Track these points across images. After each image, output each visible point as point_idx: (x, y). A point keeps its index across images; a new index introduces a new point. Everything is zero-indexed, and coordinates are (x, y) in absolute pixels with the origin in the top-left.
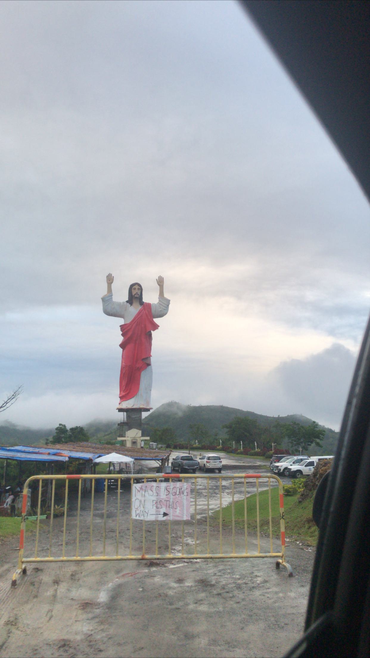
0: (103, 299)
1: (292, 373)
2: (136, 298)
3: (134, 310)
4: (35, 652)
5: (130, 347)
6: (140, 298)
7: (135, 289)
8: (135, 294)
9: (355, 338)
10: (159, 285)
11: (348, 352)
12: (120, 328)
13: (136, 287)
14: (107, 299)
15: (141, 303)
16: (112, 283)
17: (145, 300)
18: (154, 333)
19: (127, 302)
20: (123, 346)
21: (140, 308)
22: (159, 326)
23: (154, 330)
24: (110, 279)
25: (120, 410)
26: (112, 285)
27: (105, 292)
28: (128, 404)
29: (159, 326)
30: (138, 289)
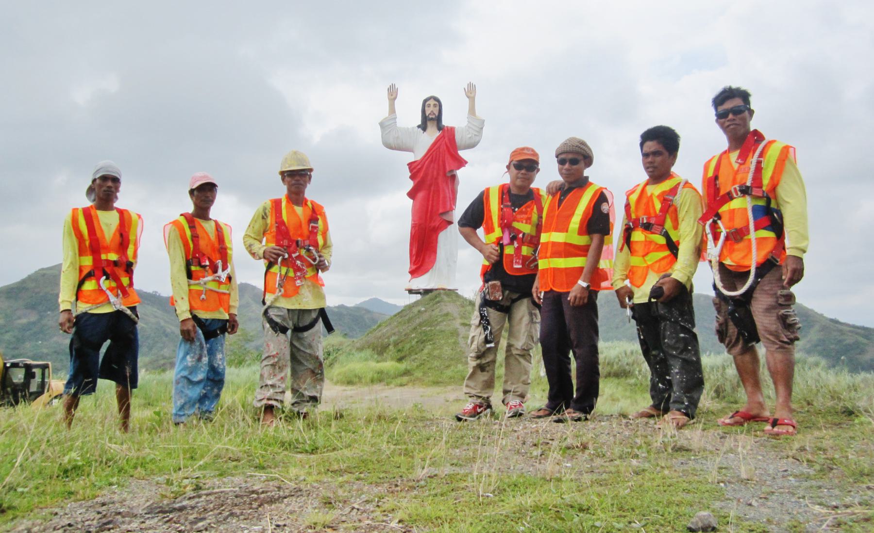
0: (382, 125)
1: (85, 399)
2: (432, 119)
3: (431, 136)
4: (618, 344)
5: (421, 195)
6: (438, 119)
7: (429, 106)
8: (431, 116)
9: (631, 340)
10: (468, 97)
11: (254, 288)
12: (407, 167)
13: (432, 102)
14: (387, 123)
15: (440, 127)
16: (395, 99)
17: (446, 122)
18: (460, 173)
19: (419, 127)
20: (412, 194)
21: (438, 134)
22: (466, 162)
23: (459, 168)
24: (393, 93)
25: (411, 291)
26: (396, 101)
27: (385, 113)
28: (423, 282)
29: (466, 162)
30: (435, 105)
